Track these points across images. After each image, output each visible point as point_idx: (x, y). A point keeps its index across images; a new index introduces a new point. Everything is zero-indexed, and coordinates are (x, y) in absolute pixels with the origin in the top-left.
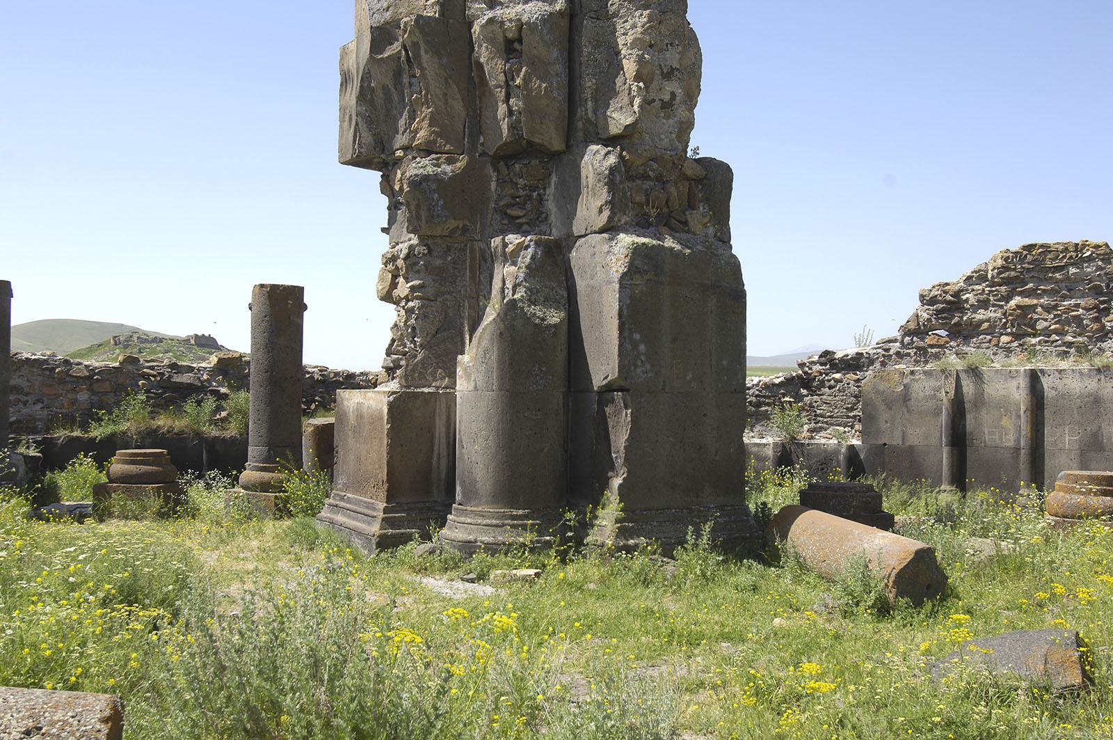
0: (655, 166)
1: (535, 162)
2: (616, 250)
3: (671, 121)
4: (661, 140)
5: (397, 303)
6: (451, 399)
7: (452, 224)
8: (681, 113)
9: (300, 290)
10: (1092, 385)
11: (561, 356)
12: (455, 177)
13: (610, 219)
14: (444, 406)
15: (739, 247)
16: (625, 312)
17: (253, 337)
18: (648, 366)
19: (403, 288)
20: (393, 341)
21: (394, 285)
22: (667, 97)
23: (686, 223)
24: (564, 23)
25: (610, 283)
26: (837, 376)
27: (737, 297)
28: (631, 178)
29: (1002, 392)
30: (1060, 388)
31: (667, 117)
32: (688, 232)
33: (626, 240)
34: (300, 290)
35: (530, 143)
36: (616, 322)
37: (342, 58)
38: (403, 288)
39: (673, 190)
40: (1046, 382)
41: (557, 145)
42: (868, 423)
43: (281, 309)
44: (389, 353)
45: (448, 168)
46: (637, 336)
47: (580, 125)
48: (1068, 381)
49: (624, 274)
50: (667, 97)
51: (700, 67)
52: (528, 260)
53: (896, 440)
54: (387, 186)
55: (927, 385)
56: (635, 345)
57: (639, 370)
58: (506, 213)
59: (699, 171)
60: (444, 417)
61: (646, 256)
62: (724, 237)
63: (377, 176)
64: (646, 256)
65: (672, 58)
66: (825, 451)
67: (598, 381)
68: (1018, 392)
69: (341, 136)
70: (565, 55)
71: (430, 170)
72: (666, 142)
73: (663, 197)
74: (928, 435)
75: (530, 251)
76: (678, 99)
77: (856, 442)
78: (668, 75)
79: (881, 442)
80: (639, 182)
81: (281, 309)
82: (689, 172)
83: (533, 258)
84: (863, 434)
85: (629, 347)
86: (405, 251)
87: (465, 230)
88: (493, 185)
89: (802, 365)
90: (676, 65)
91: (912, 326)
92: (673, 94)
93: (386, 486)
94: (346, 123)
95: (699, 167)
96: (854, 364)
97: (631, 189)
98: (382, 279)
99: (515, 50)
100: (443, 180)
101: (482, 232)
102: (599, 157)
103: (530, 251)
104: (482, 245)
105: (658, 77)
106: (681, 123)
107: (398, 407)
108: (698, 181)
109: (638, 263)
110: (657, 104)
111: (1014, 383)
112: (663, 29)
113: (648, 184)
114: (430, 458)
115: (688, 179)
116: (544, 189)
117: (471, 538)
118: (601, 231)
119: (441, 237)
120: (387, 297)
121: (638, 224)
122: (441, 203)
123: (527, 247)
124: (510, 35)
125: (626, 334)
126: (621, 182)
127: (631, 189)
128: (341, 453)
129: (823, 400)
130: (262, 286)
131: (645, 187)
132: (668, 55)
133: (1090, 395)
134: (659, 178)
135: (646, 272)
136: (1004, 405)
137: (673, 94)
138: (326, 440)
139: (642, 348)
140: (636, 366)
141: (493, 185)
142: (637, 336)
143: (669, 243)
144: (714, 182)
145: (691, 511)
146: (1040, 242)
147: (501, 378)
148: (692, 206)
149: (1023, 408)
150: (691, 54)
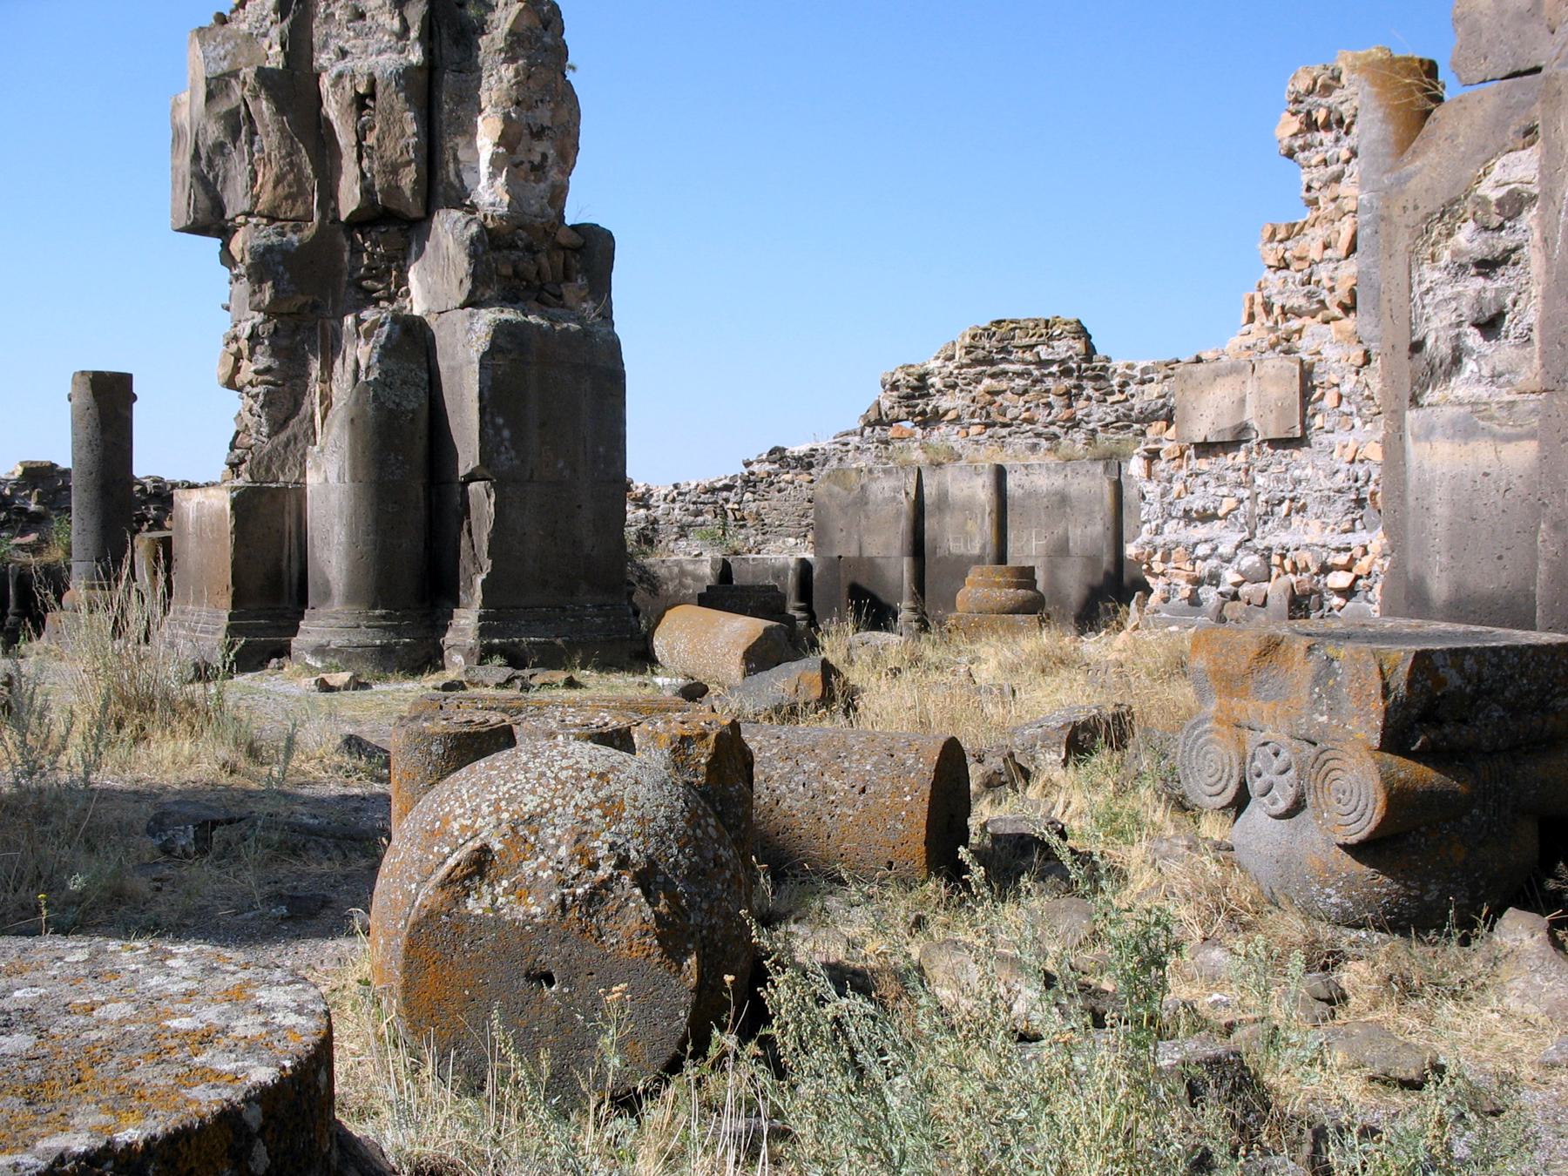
0: (524, 234)
1: (393, 229)
2: (477, 327)
3: (542, 185)
4: (530, 205)
5: (240, 390)
6: (300, 492)
7: (301, 299)
8: (554, 174)
9: (130, 376)
10: (1058, 481)
11: (420, 446)
12: (304, 247)
13: (471, 293)
14: (293, 502)
15: (625, 323)
16: (486, 395)
17: (74, 433)
18: (513, 453)
19: (248, 370)
20: (238, 433)
21: (236, 369)
22: (537, 159)
23: (560, 297)
24: (422, 78)
25: (471, 363)
26: (788, 477)
27: (616, 378)
28: (498, 248)
29: (966, 492)
30: (1027, 485)
31: (538, 181)
32: (563, 307)
33: (487, 317)
34: (130, 376)
35: (385, 209)
36: (477, 405)
37: (173, 110)
38: (248, 370)
39: (544, 260)
40: (1011, 482)
41: (416, 212)
42: (819, 532)
43: (109, 400)
44: (233, 446)
45: (295, 238)
46: (500, 421)
47: (440, 189)
48: (1034, 478)
49: (485, 355)
50: (537, 159)
51: (577, 125)
52: (383, 339)
53: (852, 552)
54: (227, 258)
55: (885, 485)
56: (498, 430)
57: (503, 457)
58: (361, 287)
59: (576, 240)
60: (294, 515)
61: (510, 334)
62: (607, 316)
63: (216, 243)
64: (510, 334)
65: (543, 115)
66: (773, 567)
67: (463, 471)
68: (981, 490)
69: (174, 200)
70: (424, 112)
71: (275, 239)
72: (536, 208)
73: (533, 269)
74: (885, 547)
75: (386, 328)
76: (550, 161)
77: (809, 556)
78: (538, 133)
79: (835, 555)
80: (506, 252)
81: (109, 400)
82: (563, 241)
83: (389, 337)
84: (817, 545)
85: (491, 432)
86: (248, 331)
87: (315, 306)
88: (346, 256)
89: (748, 464)
90: (547, 123)
91: (873, 416)
92: (544, 156)
93: (231, 590)
94: (179, 186)
95: (575, 235)
96: (806, 463)
97: (496, 261)
98: (223, 363)
99: (368, 107)
100: (288, 251)
101: (333, 309)
102: (460, 225)
103: (386, 328)
104: (334, 323)
105: (526, 139)
106: (554, 186)
107: (244, 505)
108: (576, 250)
109: (501, 341)
110: (526, 166)
111: (979, 481)
112: (531, 84)
113: (515, 255)
114: (279, 560)
115: (564, 248)
116: (405, 259)
117: (324, 641)
118: (462, 307)
119: (289, 314)
120: (230, 384)
121: (504, 299)
122: (287, 276)
123: (382, 325)
124: (361, 90)
125: (488, 418)
126: (484, 252)
127: (496, 261)
128: (180, 561)
129: (773, 506)
130: (83, 373)
131: (513, 257)
132: (538, 112)
133: (1056, 493)
134: (529, 248)
135: (510, 351)
136: (968, 507)
137: (544, 156)
138: (165, 552)
139: (506, 433)
140: (499, 453)
141: (346, 256)
142: (500, 421)
143: (531, 319)
144: (592, 252)
145: (564, 609)
146: (1008, 317)
147: (354, 467)
148: (567, 277)
149: (988, 509)
150: (564, 114)
